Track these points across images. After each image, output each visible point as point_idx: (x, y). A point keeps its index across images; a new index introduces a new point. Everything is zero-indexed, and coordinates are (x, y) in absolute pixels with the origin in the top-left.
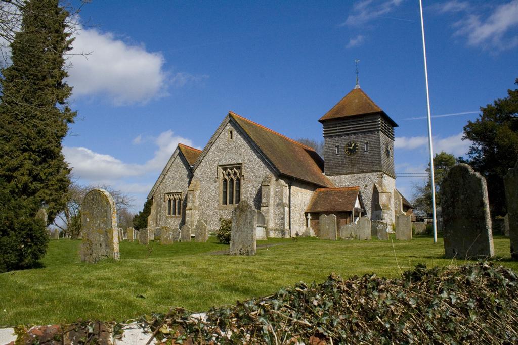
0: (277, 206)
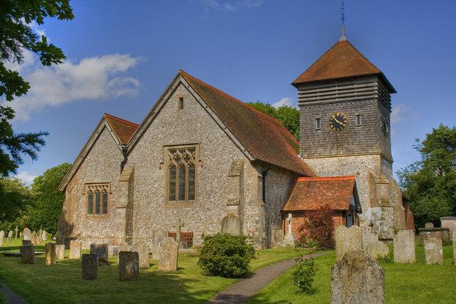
0: (250, 205)
